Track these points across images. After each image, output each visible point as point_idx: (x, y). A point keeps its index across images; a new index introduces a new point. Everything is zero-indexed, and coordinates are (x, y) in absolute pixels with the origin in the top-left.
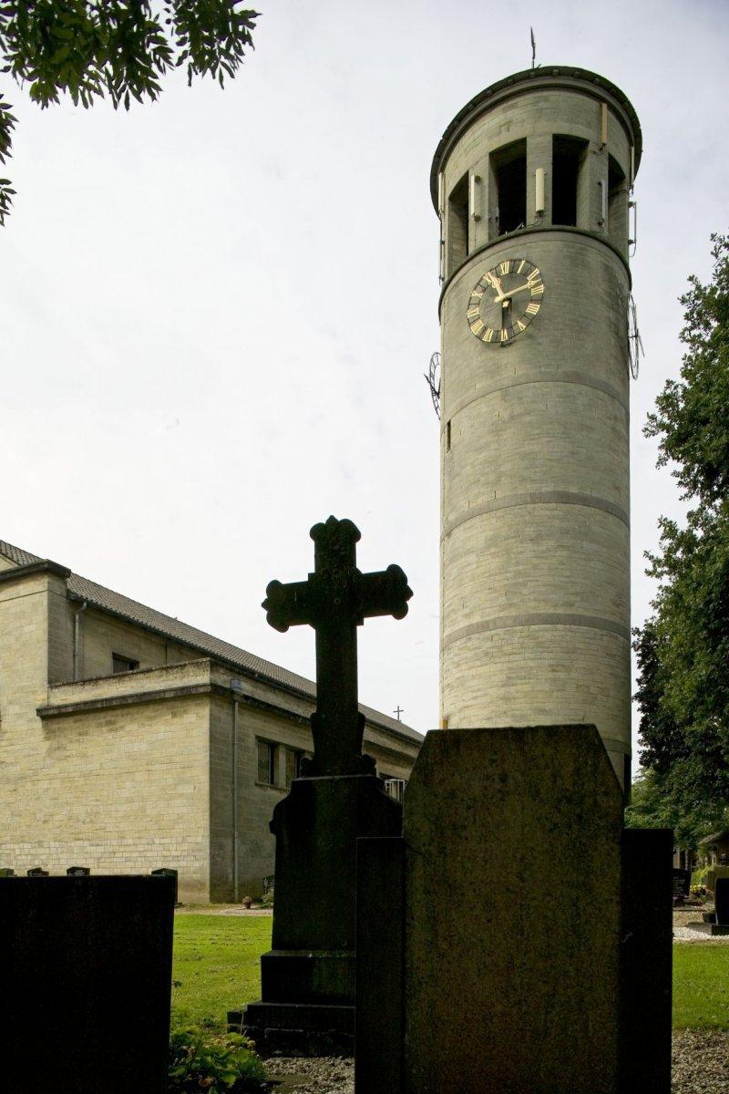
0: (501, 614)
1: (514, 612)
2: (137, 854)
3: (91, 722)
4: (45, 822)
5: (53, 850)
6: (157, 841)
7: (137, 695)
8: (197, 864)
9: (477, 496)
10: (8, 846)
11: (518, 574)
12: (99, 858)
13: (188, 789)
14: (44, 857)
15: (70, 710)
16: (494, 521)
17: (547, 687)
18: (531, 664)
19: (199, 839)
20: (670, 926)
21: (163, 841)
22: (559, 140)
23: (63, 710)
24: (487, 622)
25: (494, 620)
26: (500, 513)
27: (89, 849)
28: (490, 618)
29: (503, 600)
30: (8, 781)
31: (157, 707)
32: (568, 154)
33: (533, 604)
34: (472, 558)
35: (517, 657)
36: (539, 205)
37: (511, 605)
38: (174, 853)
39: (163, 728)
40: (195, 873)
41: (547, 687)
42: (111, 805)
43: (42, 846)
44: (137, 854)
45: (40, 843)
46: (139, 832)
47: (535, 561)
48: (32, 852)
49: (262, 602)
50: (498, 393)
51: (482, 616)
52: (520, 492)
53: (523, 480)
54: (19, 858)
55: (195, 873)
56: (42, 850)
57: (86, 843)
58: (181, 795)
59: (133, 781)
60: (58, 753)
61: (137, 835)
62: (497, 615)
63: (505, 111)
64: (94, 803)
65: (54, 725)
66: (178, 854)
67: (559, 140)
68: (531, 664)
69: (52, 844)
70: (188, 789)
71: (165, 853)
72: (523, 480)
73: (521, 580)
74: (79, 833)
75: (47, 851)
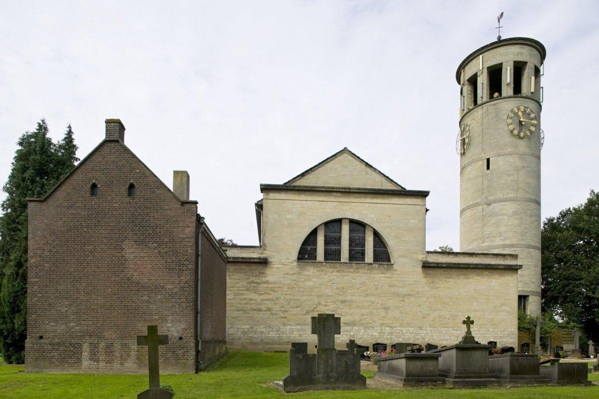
0: (519, 243)
1: (524, 243)
2: (479, 335)
3: (454, 272)
4: (423, 317)
5: (429, 332)
6: (491, 330)
7: (484, 265)
8: (512, 340)
9: (509, 193)
10: (398, 328)
11: (525, 228)
12: (458, 336)
13: (508, 308)
14: (423, 335)
15: (445, 266)
16: (516, 205)
17: (533, 273)
18: (529, 263)
19: (513, 330)
20: (158, 371)
21: (494, 330)
22: (516, 63)
23: (440, 265)
24: (513, 245)
25: (517, 244)
26: (519, 203)
27: (451, 332)
28: (515, 243)
29: (519, 237)
30: (398, 295)
31: (491, 271)
32: (519, 68)
33: (530, 241)
34: (506, 217)
35: (526, 260)
36: (508, 81)
37: (523, 240)
38: (499, 335)
39: (494, 281)
40: (510, 344)
41: (533, 273)
42: (465, 312)
43: (422, 329)
44: (479, 335)
45: (421, 328)
46: (480, 325)
47: (531, 224)
48: (415, 331)
49: (176, 170)
50: (518, 156)
51: (510, 242)
52: (526, 197)
53: (527, 192)
54: (405, 334)
55: (510, 344)
56: (422, 332)
57: (450, 329)
58: (503, 311)
59: (477, 302)
60: (432, 285)
61: (480, 326)
62: (517, 243)
63: (520, 48)
64: (455, 311)
65: (431, 272)
66: (502, 335)
67: (516, 63)
68: (529, 263)
69: (428, 329)
70: (508, 308)
71: (495, 335)
72: (527, 192)
73: (526, 231)
74: (446, 324)
75: (425, 332)
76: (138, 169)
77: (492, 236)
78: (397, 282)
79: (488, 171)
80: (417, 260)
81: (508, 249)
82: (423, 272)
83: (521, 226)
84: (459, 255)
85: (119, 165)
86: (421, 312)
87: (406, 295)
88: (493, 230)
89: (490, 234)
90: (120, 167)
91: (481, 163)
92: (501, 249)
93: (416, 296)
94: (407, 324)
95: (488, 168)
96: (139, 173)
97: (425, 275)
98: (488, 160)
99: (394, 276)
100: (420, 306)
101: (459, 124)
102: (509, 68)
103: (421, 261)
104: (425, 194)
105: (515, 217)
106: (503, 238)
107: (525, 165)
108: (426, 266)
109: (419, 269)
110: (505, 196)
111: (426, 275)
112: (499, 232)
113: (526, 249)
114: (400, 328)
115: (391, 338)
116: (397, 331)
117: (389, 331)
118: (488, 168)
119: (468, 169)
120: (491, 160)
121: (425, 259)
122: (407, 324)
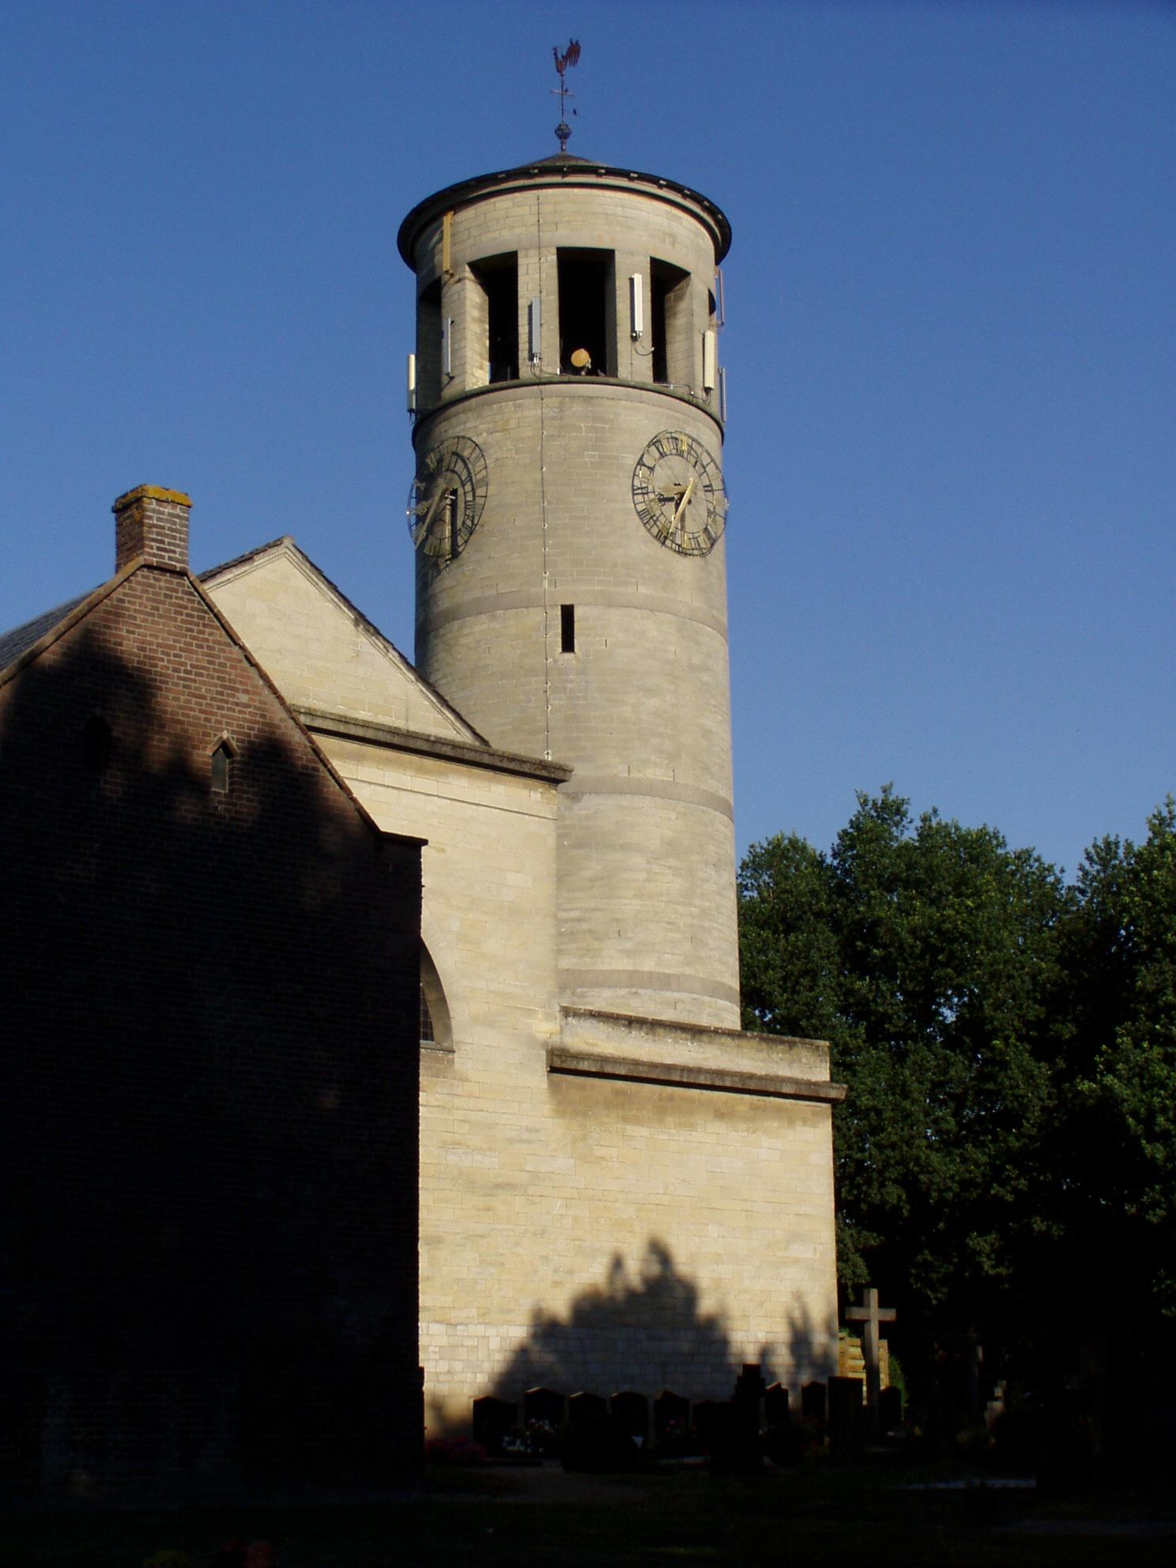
0: (687, 971)
16: (673, 816)
39: (765, 1141)
76: (246, 692)
77: (590, 932)
78: (466, 1128)
79: (568, 656)
80: (531, 1041)
81: (650, 992)
82: (554, 1088)
83: (691, 905)
84: (661, 1031)
85: (185, 664)
86: (546, 1259)
87: (498, 1186)
88: (592, 905)
89: (579, 920)
90: (186, 672)
91: (535, 616)
92: (623, 992)
93: (531, 1191)
94: (503, 1311)
95: (568, 645)
96: (246, 706)
97: (559, 1103)
98: (568, 613)
99: (457, 1101)
100: (543, 1233)
101: (407, 424)
102: (638, 279)
103: (545, 1043)
104: (559, 775)
105: (672, 862)
106: (629, 945)
107: (696, 661)
108: (563, 1065)
109: (538, 1078)
110: (635, 775)
111: (564, 1107)
112: (618, 920)
113: (707, 999)
114: (480, 1330)
115: (449, 1372)
116: (468, 1342)
117: (444, 1341)
118: (568, 645)
119: (477, 629)
120: (578, 613)
121: (556, 1040)
122: (503, 1311)
